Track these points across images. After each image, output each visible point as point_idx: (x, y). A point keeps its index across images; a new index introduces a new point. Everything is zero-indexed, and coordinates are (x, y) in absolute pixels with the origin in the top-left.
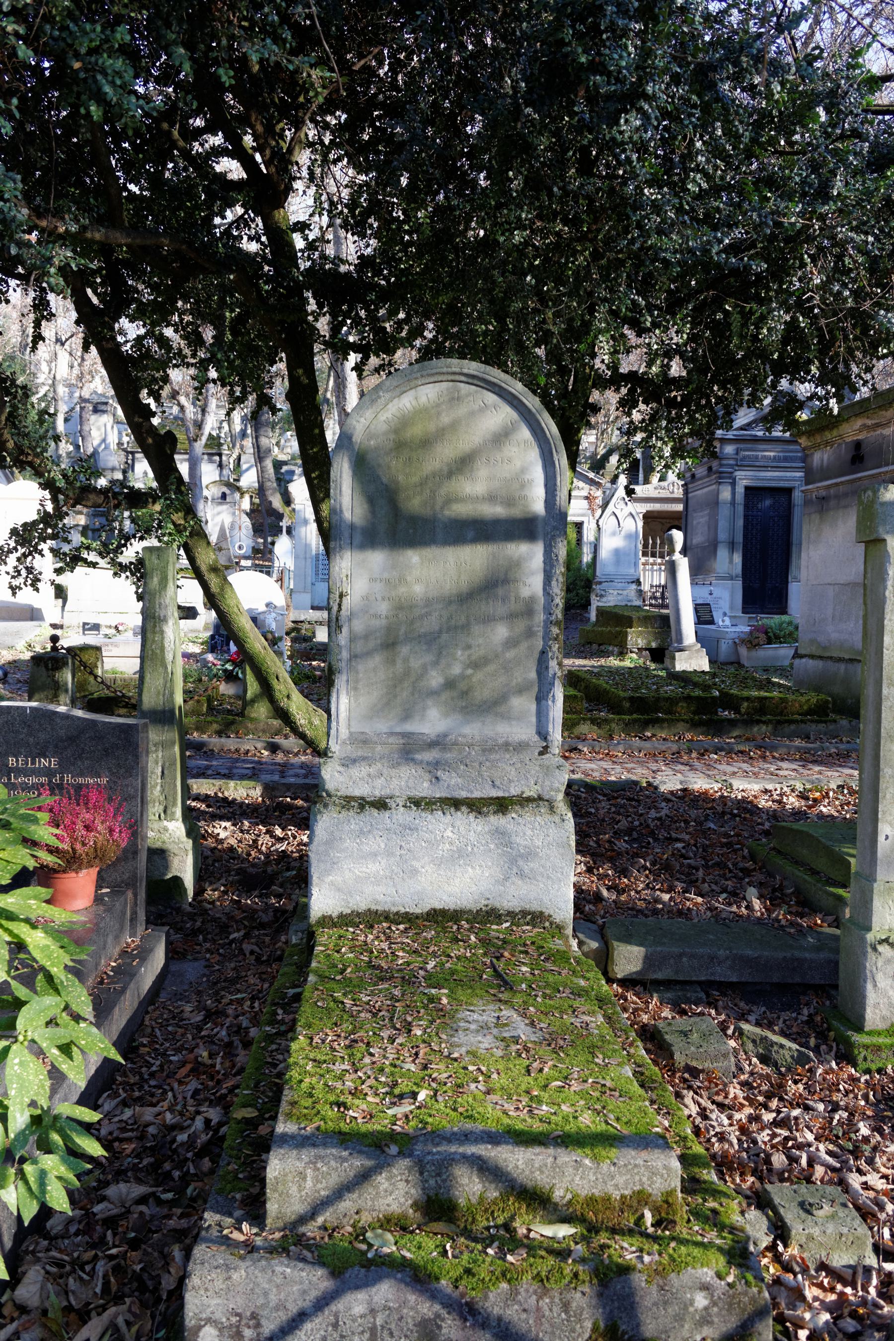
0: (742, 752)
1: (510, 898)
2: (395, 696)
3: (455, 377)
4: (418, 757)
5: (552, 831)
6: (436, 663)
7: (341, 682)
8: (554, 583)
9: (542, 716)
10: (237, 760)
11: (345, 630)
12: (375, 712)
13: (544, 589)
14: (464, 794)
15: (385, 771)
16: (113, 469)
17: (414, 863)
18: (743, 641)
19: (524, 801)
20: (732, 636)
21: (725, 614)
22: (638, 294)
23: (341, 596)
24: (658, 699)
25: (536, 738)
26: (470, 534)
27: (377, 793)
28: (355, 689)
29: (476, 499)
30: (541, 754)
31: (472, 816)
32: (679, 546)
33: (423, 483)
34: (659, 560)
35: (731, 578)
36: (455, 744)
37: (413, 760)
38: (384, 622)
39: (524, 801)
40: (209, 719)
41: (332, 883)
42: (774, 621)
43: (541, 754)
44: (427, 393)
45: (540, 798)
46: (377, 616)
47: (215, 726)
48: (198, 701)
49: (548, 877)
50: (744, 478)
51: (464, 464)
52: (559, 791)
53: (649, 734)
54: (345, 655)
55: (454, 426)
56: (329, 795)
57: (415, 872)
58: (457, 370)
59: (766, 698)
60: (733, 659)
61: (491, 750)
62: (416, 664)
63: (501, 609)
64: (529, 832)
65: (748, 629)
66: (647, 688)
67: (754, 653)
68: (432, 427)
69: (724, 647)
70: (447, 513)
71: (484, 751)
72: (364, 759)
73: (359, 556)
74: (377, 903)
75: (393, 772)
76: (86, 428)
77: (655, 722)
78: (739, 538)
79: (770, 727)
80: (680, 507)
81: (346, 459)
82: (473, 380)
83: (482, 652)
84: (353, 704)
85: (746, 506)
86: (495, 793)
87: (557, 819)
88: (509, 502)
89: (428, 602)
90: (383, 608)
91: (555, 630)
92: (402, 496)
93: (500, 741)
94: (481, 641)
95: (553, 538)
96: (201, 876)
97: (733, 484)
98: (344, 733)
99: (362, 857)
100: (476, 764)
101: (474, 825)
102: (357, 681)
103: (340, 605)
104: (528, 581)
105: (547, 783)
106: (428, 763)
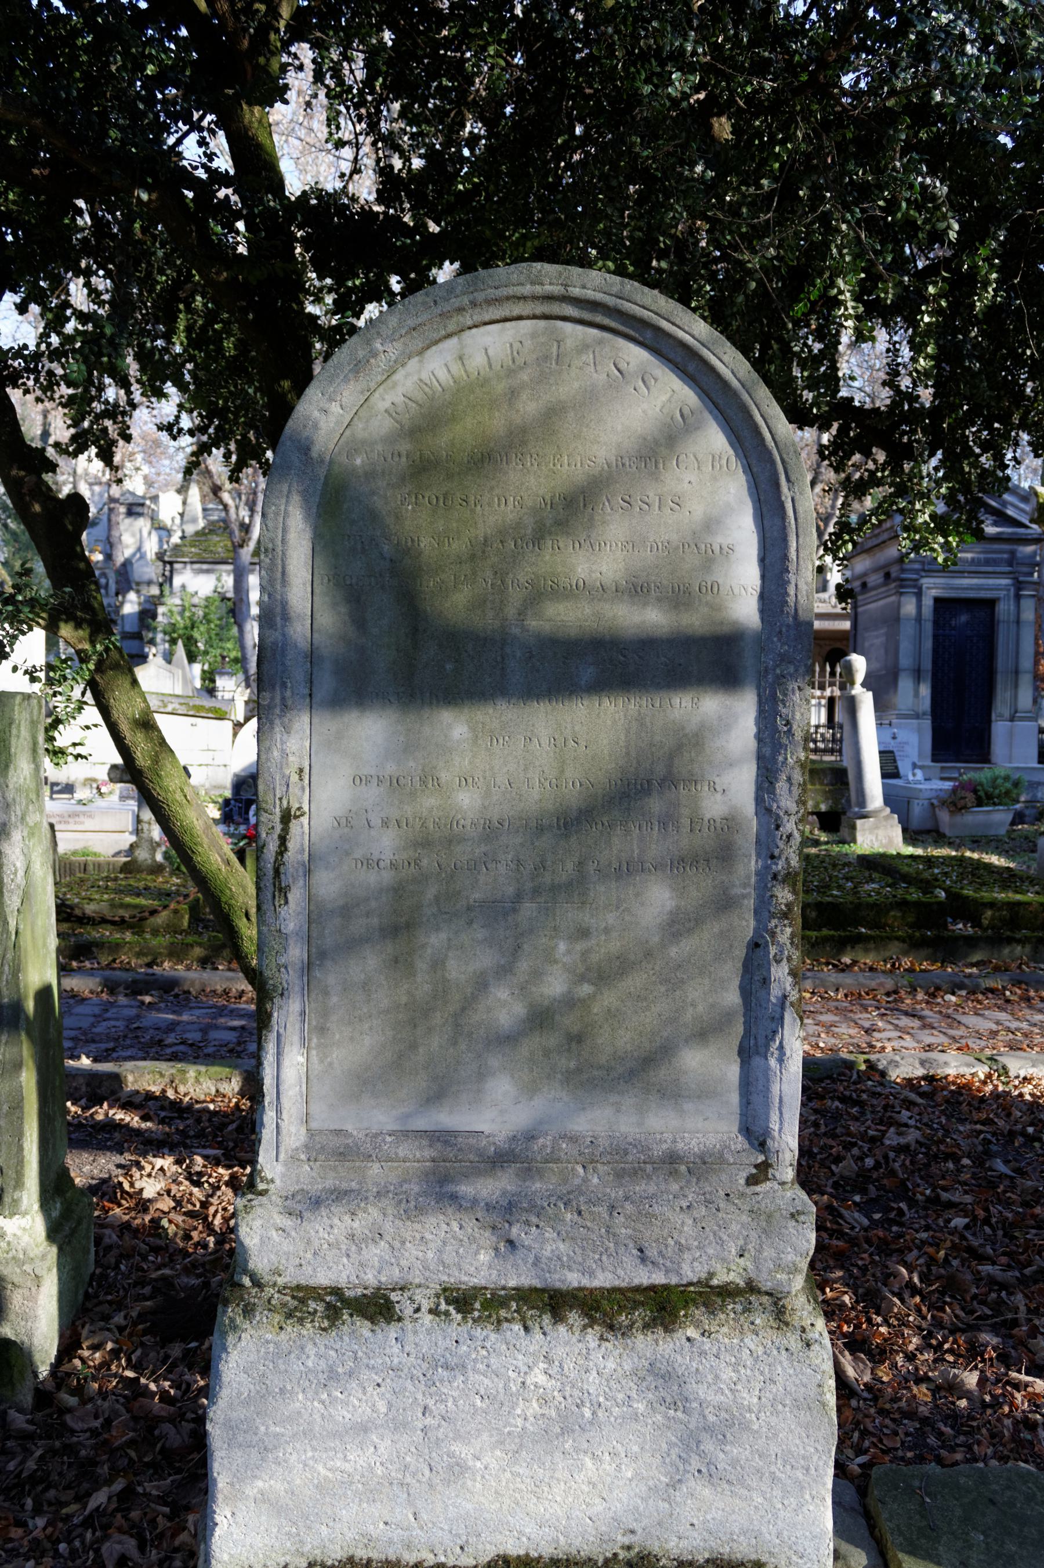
0: (992, 991)
1: (684, 1528)
2: (413, 1046)
3: (552, 308)
4: (466, 1189)
5: (783, 1368)
6: (504, 971)
7: (288, 1015)
8: (781, 786)
9: (753, 1091)
10: (222, 1011)
11: (296, 896)
12: (365, 1083)
13: (759, 800)
14: (573, 1279)
15: (388, 1227)
16: (149, 583)
17: (456, 1448)
18: (943, 803)
19: (712, 1296)
20: (928, 795)
21: (915, 766)
22: (932, 173)
23: (287, 817)
24: (858, 907)
25: (740, 1142)
26: (588, 673)
27: (371, 1278)
28: (322, 1030)
29: (599, 592)
30: (752, 1181)
31: (592, 1337)
32: (860, 676)
33: (475, 556)
34: (818, 693)
35: (917, 716)
36: (553, 1158)
37: (454, 1197)
38: (387, 877)
39: (712, 1296)
40: (190, 939)
41: (263, 1498)
42: (981, 775)
43: (752, 1181)
44: (490, 345)
45: (751, 1288)
46: (368, 862)
47: (198, 951)
48: (176, 912)
49: (774, 1479)
50: (933, 587)
51: (573, 510)
52: (794, 1270)
53: (847, 960)
54: (296, 953)
55: (553, 414)
56: (257, 1283)
57: (458, 1470)
58: (556, 289)
59: (1019, 904)
60: (929, 825)
61: (636, 1173)
62: (459, 970)
63: (658, 846)
64: (727, 1374)
65: (948, 785)
66: (840, 887)
67: (958, 819)
68: (497, 423)
69: (917, 810)
70: (533, 623)
71: (619, 1175)
72: (339, 1195)
73: (328, 724)
74: (370, 1541)
75: (410, 1230)
76: (115, 533)
77: (856, 941)
78: (927, 664)
79: (1028, 948)
80: (846, 625)
81: (296, 498)
82: (596, 313)
83: (614, 946)
84: (317, 1066)
85: (936, 623)
86: (644, 1277)
87: (793, 1340)
88: (679, 597)
89: (491, 832)
90: (386, 844)
91: (784, 895)
92: (429, 584)
93: (657, 1151)
94: (611, 918)
95: (780, 681)
96: (78, 1315)
97: (919, 595)
98: (294, 1135)
99: (334, 1435)
100: (602, 1210)
101: (597, 1356)
102: (325, 1013)
103: (283, 840)
104: (721, 782)
105: (768, 1253)
106: (489, 1207)
